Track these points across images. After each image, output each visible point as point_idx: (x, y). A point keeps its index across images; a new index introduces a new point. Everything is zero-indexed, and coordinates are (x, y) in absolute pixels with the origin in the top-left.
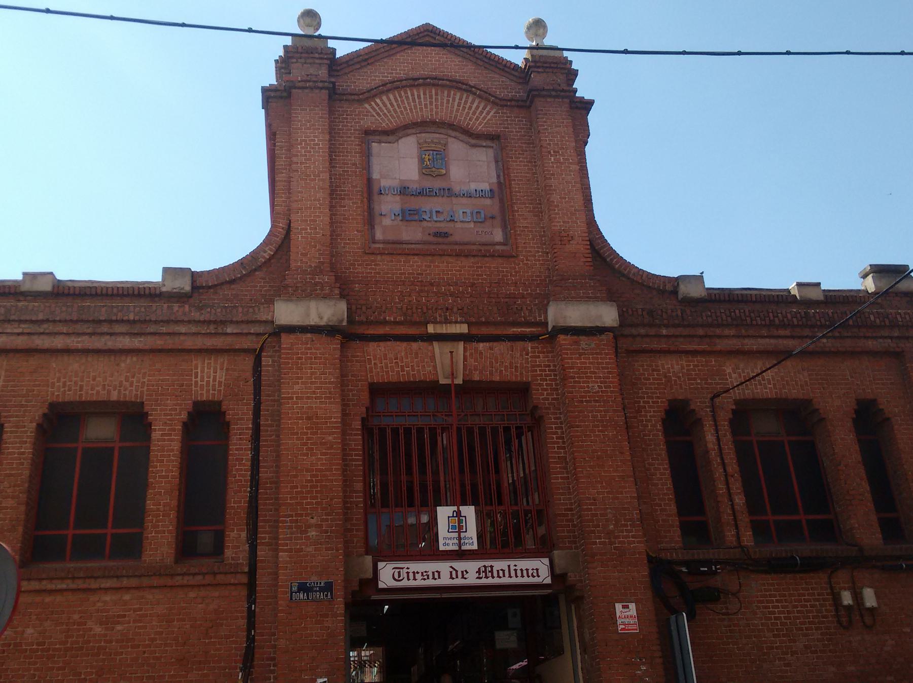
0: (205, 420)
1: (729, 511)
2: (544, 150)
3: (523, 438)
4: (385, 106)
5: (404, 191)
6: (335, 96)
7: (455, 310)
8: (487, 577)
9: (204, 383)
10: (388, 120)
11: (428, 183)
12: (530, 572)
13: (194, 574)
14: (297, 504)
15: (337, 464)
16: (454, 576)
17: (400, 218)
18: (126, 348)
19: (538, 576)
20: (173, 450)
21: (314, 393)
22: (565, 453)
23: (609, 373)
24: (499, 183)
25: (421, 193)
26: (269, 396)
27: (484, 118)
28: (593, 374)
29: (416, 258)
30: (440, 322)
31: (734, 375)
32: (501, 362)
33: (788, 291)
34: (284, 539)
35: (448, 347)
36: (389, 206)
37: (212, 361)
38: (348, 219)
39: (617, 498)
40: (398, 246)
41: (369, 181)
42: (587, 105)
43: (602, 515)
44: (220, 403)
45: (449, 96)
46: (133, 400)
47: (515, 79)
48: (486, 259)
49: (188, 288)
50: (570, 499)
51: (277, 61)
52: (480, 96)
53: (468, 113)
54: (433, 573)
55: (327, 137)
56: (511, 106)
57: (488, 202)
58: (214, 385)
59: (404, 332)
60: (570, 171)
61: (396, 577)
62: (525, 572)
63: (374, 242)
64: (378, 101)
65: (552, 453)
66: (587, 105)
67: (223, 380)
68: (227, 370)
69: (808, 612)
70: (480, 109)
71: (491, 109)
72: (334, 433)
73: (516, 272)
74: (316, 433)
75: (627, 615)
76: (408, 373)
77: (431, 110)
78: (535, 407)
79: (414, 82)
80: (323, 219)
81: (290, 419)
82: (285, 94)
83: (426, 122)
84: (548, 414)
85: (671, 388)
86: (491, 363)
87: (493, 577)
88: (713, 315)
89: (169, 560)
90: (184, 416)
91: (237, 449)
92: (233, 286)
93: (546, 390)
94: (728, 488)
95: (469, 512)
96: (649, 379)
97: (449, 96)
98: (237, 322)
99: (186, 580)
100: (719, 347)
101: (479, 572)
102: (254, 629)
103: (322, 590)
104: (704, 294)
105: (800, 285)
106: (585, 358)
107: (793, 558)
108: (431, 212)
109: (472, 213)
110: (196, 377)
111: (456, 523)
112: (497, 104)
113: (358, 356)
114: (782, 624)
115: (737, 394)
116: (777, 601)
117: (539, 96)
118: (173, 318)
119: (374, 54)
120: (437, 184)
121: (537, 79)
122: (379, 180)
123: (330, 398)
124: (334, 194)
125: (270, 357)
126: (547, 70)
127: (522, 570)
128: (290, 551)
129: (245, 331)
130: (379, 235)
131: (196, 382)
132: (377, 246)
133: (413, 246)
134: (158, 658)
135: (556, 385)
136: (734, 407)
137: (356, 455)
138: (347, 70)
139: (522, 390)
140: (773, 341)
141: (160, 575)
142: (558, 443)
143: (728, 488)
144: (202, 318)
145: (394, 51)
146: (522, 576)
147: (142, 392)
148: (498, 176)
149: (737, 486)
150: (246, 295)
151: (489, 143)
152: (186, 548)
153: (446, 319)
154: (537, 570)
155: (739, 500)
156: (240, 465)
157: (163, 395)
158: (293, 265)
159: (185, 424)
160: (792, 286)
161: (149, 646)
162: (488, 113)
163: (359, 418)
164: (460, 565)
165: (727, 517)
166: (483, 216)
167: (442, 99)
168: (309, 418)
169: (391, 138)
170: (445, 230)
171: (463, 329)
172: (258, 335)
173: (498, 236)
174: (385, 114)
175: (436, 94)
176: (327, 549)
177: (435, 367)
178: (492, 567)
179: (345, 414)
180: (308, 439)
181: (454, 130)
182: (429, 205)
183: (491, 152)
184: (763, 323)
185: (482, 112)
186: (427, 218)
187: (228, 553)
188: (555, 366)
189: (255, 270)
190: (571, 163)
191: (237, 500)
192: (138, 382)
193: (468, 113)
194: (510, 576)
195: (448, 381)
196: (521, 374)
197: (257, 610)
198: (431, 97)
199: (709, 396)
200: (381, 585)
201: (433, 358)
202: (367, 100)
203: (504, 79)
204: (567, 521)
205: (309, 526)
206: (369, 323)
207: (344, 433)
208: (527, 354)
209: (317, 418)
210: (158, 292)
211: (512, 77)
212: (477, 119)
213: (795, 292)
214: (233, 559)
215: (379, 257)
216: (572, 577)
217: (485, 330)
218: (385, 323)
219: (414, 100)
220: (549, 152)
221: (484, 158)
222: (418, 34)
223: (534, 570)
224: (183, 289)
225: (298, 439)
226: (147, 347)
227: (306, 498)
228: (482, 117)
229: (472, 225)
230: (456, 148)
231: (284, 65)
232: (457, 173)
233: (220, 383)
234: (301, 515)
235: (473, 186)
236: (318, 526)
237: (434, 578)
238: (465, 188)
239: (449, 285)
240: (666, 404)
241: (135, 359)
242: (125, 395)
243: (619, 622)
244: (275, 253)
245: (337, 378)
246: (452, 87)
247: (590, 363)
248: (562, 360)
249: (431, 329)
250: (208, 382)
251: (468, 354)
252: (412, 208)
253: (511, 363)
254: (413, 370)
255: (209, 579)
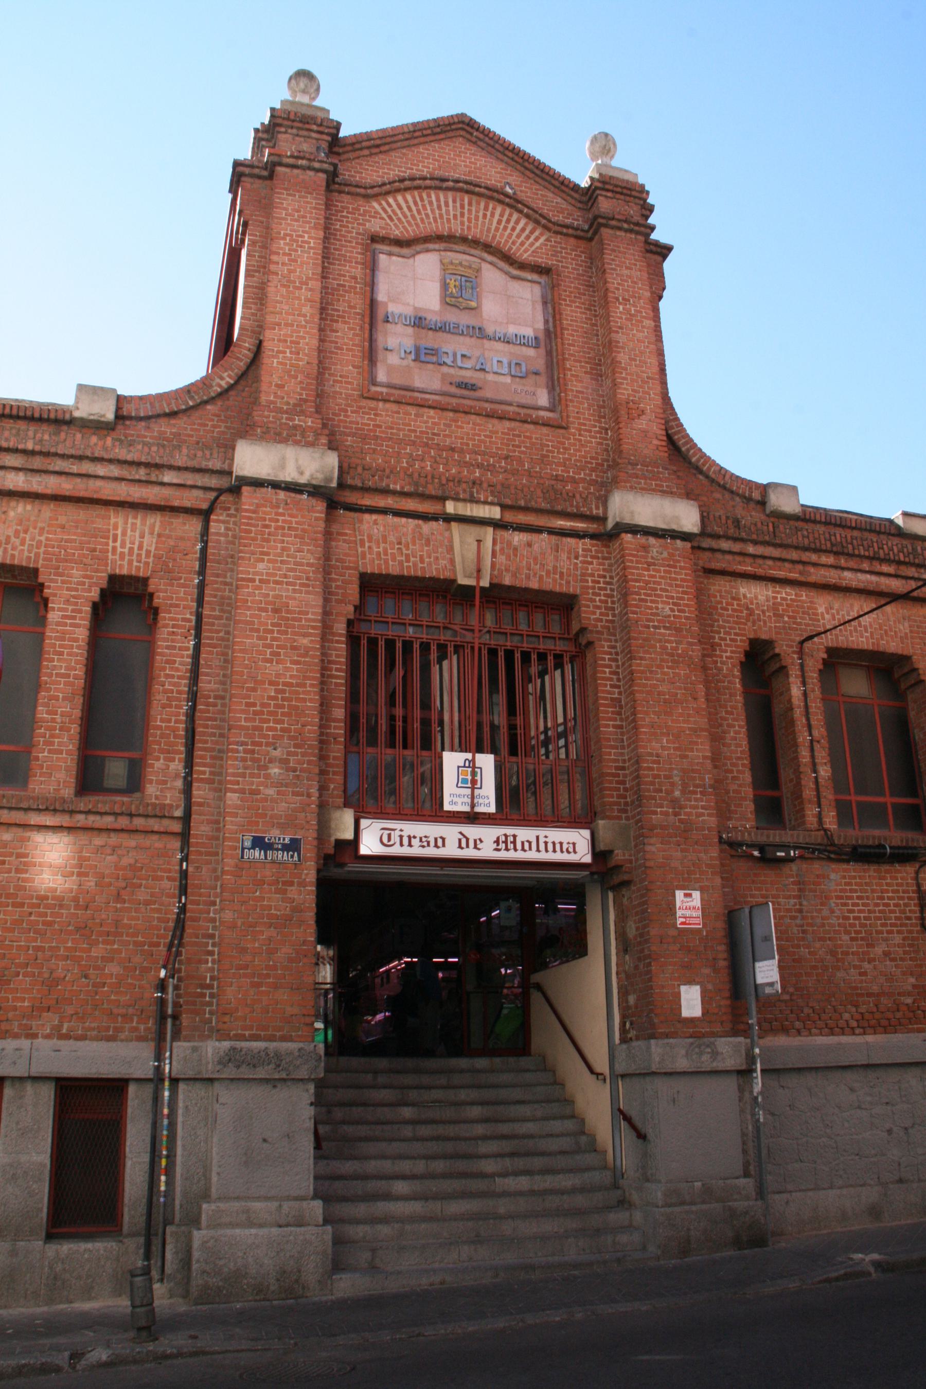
0: (123, 601)
1: (812, 786)
2: (610, 295)
3: (547, 678)
4: (400, 208)
5: (418, 322)
6: (333, 183)
7: (485, 485)
8: (507, 849)
9: (126, 550)
10: (404, 227)
11: (453, 317)
12: (565, 847)
13: (102, 814)
14: (255, 728)
15: (313, 678)
16: (464, 844)
17: (413, 356)
18: (19, 489)
19: (575, 852)
20: (76, 640)
21: (286, 576)
22: (620, 693)
23: (684, 593)
24: (547, 332)
25: (442, 328)
26: (218, 576)
27: (532, 245)
28: (664, 592)
29: (432, 412)
30: (464, 500)
31: (827, 616)
32: (543, 561)
33: (891, 521)
34: (234, 775)
35: (473, 532)
36: (397, 340)
37: (139, 522)
38: (342, 349)
39: (686, 757)
40: (409, 394)
41: (373, 304)
42: (664, 251)
43: (666, 777)
44: (145, 581)
45: (486, 208)
46: (24, 564)
47: (573, 202)
48: (526, 425)
49: (110, 416)
50: (622, 754)
51: (257, 131)
52: (527, 216)
53: (510, 236)
54: (436, 839)
55: (321, 234)
56: (566, 235)
57: (531, 352)
58: (139, 555)
59: (412, 508)
60: (643, 327)
61: (385, 840)
62: (558, 847)
63: (375, 384)
64: (391, 200)
65: (603, 692)
66: (664, 251)
67: (153, 549)
68: (159, 535)
69: (891, 912)
70: (527, 232)
71: (542, 234)
72: (311, 635)
73: (565, 448)
74: (286, 633)
75: (689, 906)
76: (415, 565)
77: (462, 224)
78: (583, 630)
79: (440, 183)
80: (309, 342)
81: (249, 608)
82: (265, 173)
83: (455, 237)
84: (600, 640)
85: (754, 623)
86: (528, 564)
87: (516, 850)
88: (811, 536)
89: (68, 792)
90: (95, 594)
91: (168, 647)
92: (173, 422)
93: (599, 607)
94: (813, 757)
95: (486, 762)
96: (727, 610)
97: (486, 208)
98: (179, 469)
99: (93, 820)
100: (812, 579)
101: (497, 842)
102: (186, 895)
103: (286, 848)
104: (797, 510)
105: (906, 514)
106: (654, 570)
107: (884, 847)
108: (455, 355)
109: (510, 365)
110: (115, 540)
111: (466, 776)
112: (549, 230)
113: (346, 534)
114: (862, 925)
115: (829, 640)
116: (858, 898)
117: (606, 226)
118: (89, 454)
119: (388, 140)
120: (465, 319)
121: (605, 205)
122: (386, 304)
123: (308, 586)
124: (325, 312)
125: (223, 522)
126: (618, 196)
127: (554, 843)
128: (242, 791)
129: (189, 483)
130: (382, 376)
131: (114, 548)
132: (379, 389)
133: (427, 396)
134: (50, 924)
135: (613, 602)
136: (825, 656)
137: (337, 670)
138: (351, 155)
139: (563, 605)
140: (874, 578)
141: (55, 810)
142: (611, 679)
143: (813, 757)
144: (129, 457)
145: (416, 141)
146: (554, 851)
147: (37, 555)
148: (546, 322)
149: (822, 755)
150: (192, 436)
151: (535, 277)
152: (89, 780)
153: (472, 495)
154: (574, 844)
155: (824, 772)
156: (171, 669)
157: (66, 561)
158: (263, 398)
159: (95, 606)
160: (895, 515)
161: (39, 906)
162: (537, 239)
163: (344, 620)
164: (473, 831)
165: (808, 792)
166: (524, 369)
167: (477, 212)
168: (276, 611)
169: (405, 251)
170: (474, 382)
171: (495, 513)
172: (206, 489)
173: (543, 399)
174: (399, 219)
175: (470, 204)
176: (294, 794)
177: (452, 561)
178: (515, 836)
179: (326, 613)
180: (273, 639)
181: (490, 253)
182: (452, 345)
183: (537, 290)
184: (867, 554)
185: (528, 238)
186: (449, 361)
187: (151, 790)
188: (611, 577)
189: (206, 402)
190: (645, 318)
191: (166, 716)
192: (32, 539)
193: (510, 236)
194: (538, 850)
195: (471, 582)
196: (568, 582)
197: (191, 869)
198: (462, 207)
199: (798, 639)
200: (364, 850)
201: (450, 549)
202: (375, 196)
203: (559, 200)
204: (618, 782)
205: (271, 761)
206: (366, 490)
207: (324, 638)
208: (576, 558)
209: (288, 612)
210: (67, 417)
211: (570, 200)
212: (522, 244)
213: (900, 522)
214: (157, 798)
215: (381, 404)
216: (620, 856)
217: (522, 518)
218: (386, 492)
219: (439, 207)
220: (617, 299)
221: (529, 296)
222: (450, 124)
223: (571, 845)
224: (104, 416)
225: (259, 638)
226: (49, 492)
227: (268, 721)
228: (530, 243)
229: (508, 380)
230: (492, 276)
231: (265, 135)
232: (491, 310)
233: (148, 553)
234: (260, 744)
235: (512, 330)
236: (284, 762)
237: (436, 846)
238: (501, 331)
239: (476, 453)
240: (747, 644)
241: (29, 507)
242: (13, 556)
243: (679, 913)
244: (237, 382)
245: (319, 559)
246: (491, 198)
247: (661, 577)
248: (625, 568)
249: (450, 507)
250: (131, 549)
251: (498, 548)
252: (429, 345)
253: (555, 568)
254: (422, 561)
255: (123, 822)
